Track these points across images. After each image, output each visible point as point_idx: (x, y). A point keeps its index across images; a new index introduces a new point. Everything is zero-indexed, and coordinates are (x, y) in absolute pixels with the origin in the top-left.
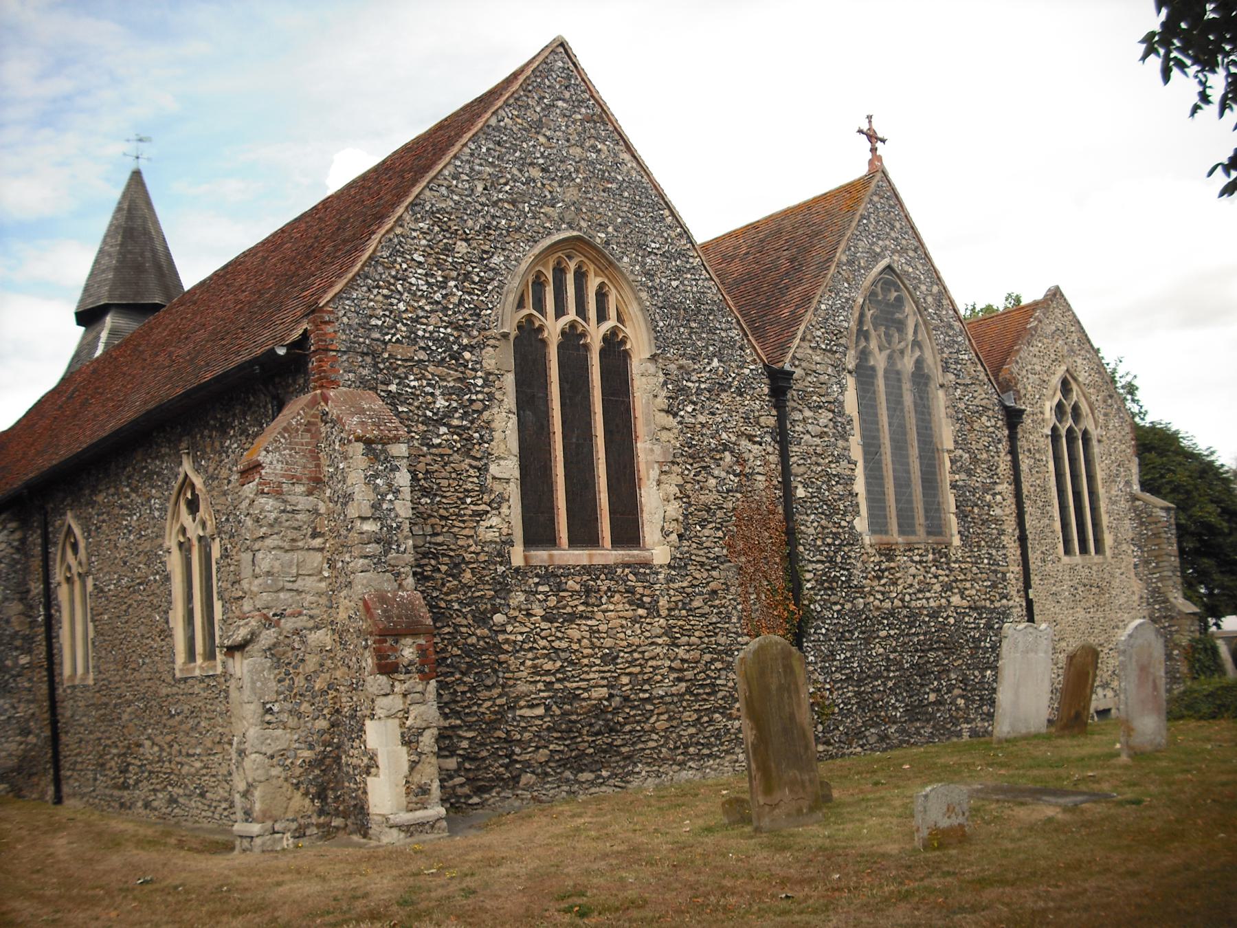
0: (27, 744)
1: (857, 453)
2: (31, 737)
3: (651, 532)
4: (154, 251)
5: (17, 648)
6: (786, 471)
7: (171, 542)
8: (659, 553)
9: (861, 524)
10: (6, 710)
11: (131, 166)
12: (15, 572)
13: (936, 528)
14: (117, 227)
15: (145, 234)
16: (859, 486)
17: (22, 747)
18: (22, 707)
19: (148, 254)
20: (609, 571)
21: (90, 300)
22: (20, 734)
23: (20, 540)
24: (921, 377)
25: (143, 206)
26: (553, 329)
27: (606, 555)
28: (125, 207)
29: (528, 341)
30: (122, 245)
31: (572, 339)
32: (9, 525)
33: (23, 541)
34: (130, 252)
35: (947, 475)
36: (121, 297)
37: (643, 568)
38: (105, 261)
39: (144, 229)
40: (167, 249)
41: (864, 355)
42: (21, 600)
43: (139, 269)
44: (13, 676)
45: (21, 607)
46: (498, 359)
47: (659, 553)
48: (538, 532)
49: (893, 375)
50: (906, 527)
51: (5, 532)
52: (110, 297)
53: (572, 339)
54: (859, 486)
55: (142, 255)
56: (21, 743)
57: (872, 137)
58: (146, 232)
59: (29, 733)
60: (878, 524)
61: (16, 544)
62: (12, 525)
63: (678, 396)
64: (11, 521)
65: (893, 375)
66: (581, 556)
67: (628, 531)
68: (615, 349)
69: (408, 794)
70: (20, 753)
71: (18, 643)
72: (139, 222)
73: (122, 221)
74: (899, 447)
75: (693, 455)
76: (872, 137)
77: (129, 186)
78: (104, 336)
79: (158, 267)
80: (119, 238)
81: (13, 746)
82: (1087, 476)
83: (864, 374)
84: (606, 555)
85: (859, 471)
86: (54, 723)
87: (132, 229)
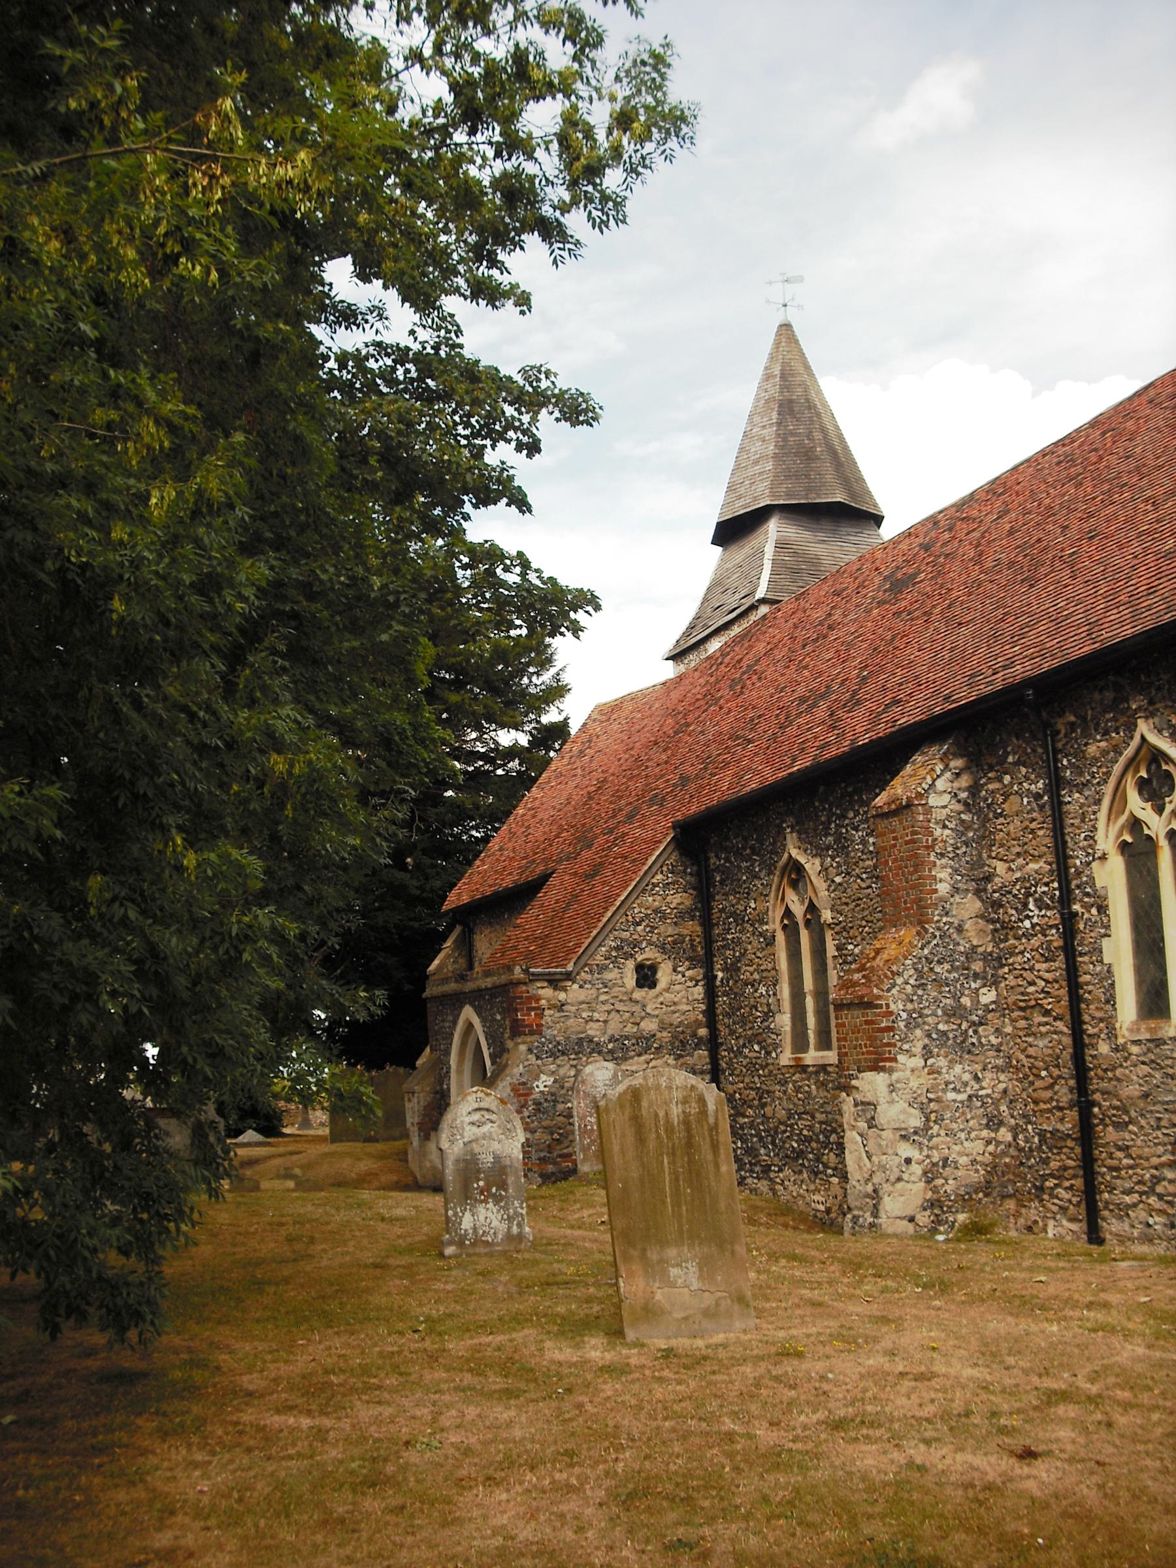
0: (998, 1143)
2: (1003, 1130)
4: (823, 430)
5: (976, 976)
10: (966, 1084)
11: (779, 319)
12: (966, 844)
14: (767, 402)
15: (809, 408)
17: (991, 1148)
18: (988, 1078)
19: (817, 435)
21: (739, 504)
22: (987, 1126)
23: (968, 789)
25: (801, 370)
28: (777, 372)
30: (779, 424)
32: (952, 764)
33: (974, 790)
34: (792, 434)
36: (789, 495)
38: (757, 447)
39: (808, 400)
40: (837, 428)
42: (978, 892)
43: (808, 455)
44: (973, 1024)
45: (978, 904)
51: (948, 775)
52: (773, 495)
55: (809, 435)
56: (988, 1143)
58: (811, 406)
59: (1001, 1123)
61: (963, 795)
62: (957, 763)
64: (956, 756)
70: (988, 1158)
71: (977, 966)
72: (799, 391)
73: (774, 391)
78: (769, 550)
79: (834, 453)
80: (775, 415)
81: (979, 1146)
86: (1084, 1104)
87: (791, 401)
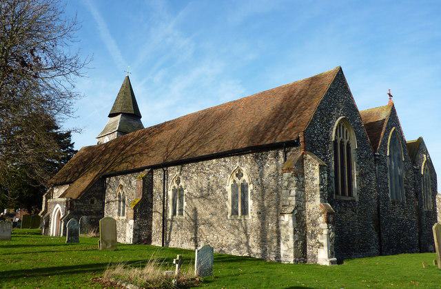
3: (355, 194)
8: (357, 200)
16: (389, 186)
47: (357, 200)
57: (390, 96)
67: (350, 194)
76: (390, 96)
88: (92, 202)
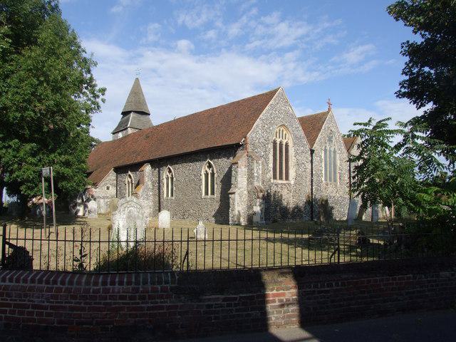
1: (323, 166)
3: (290, 178)
6: (312, 169)
7: (203, 173)
8: (292, 182)
9: (323, 179)
13: (335, 181)
20: (285, 184)
24: (335, 152)
26: (278, 141)
27: (284, 182)
29: (275, 143)
31: (281, 143)
35: (338, 171)
37: (289, 184)
41: (326, 147)
46: (271, 146)
47: (292, 182)
48: (275, 178)
49: (330, 151)
50: (330, 181)
53: (281, 143)
54: (323, 172)
60: (326, 180)
63: (297, 153)
65: (330, 151)
66: (280, 182)
67: (287, 178)
68: (287, 145)
69: (91, 79)
74: (330, 164)
75: (298, 164)
77: (266, 94)
82: (280, 171)
83: (325, 150)
84: (284, 182)
85: (323, 169)
88: (108, 188)
